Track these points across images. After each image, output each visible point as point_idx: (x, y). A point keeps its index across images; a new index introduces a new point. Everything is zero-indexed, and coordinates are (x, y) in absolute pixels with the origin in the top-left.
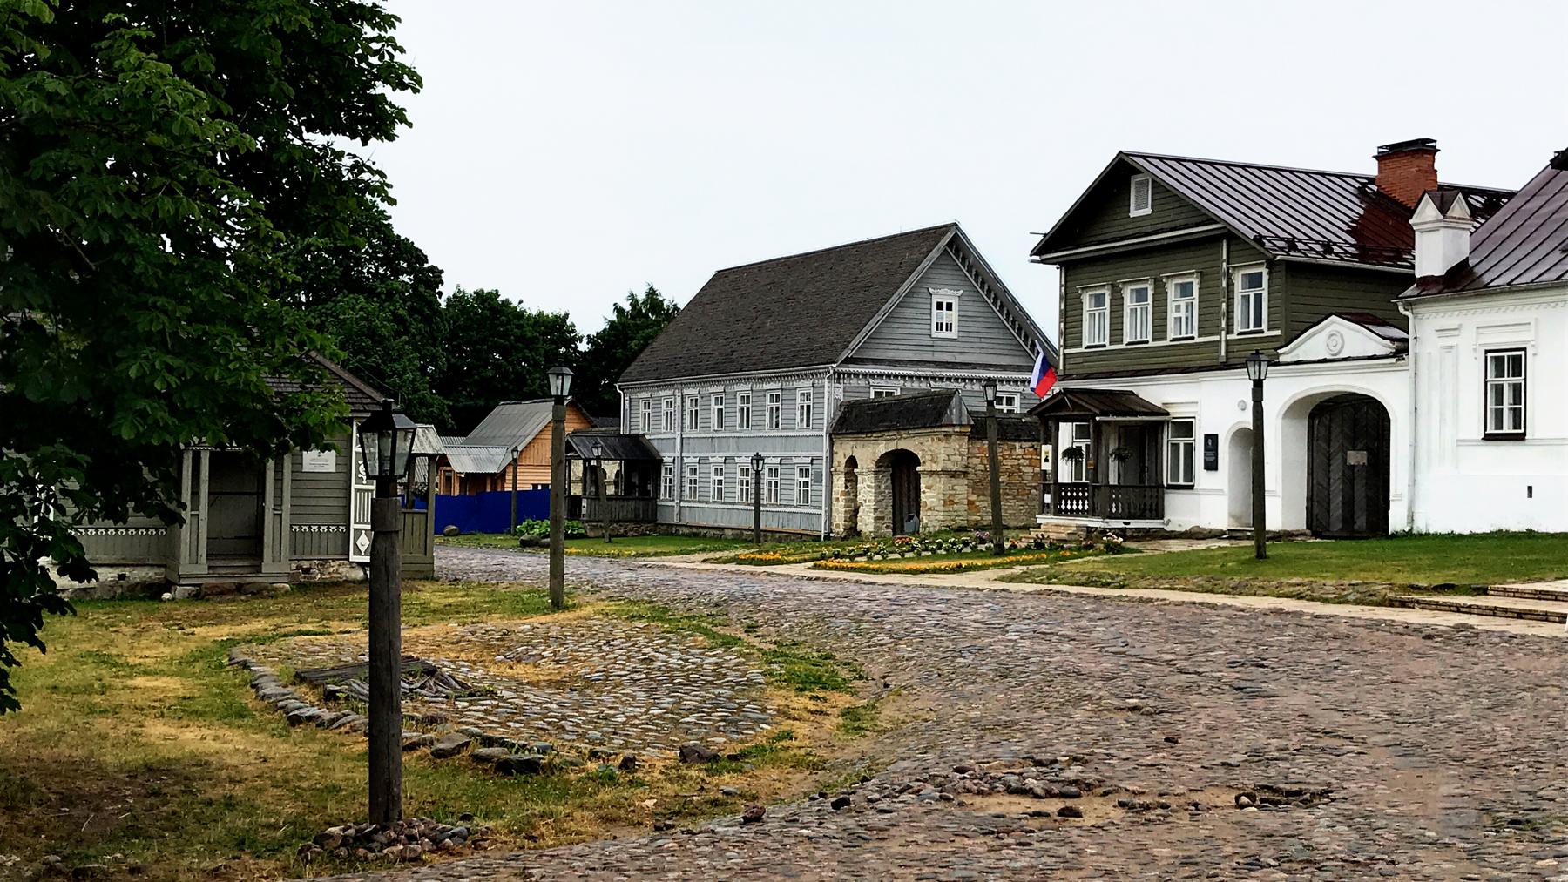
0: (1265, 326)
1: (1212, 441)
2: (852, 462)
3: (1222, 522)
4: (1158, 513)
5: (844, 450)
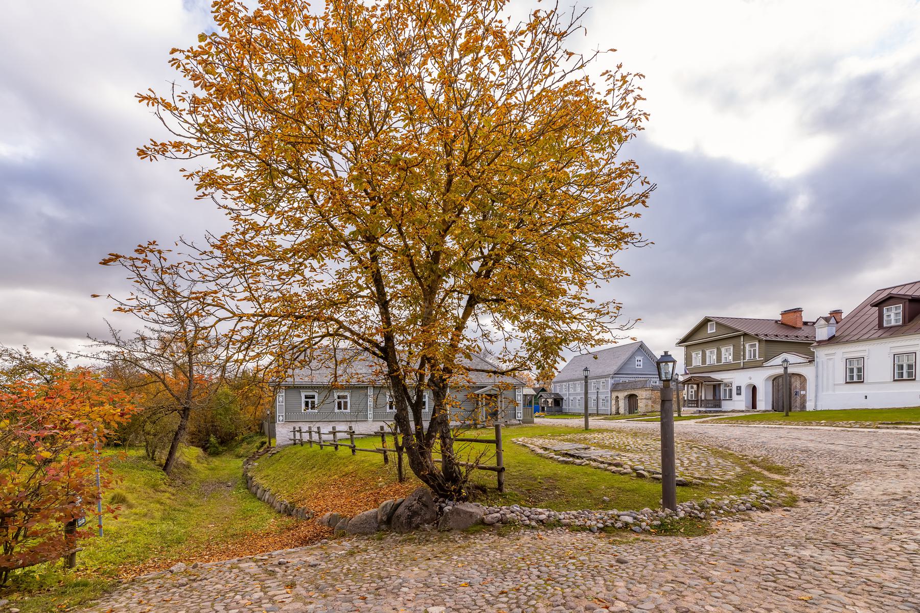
0: (757, 357)
1: (739, 389)
2: (617, 397)
3: (744, 408)
4: (720, 407)
5: (614, 395)
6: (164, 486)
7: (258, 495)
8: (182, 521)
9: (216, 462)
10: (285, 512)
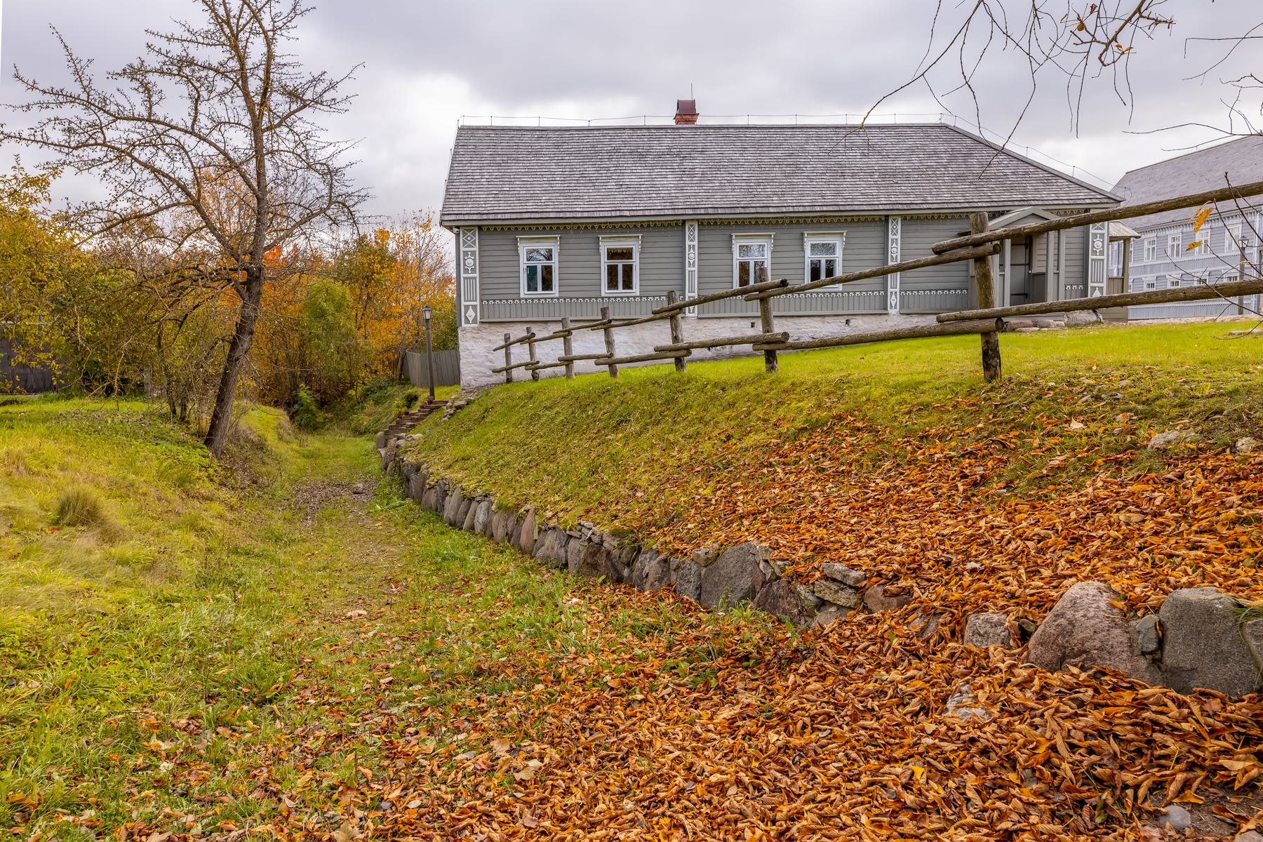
6: (208, 484)
7: (449, 512)
8: (262, 592)
9: (314, 443)
10: (594, 567)
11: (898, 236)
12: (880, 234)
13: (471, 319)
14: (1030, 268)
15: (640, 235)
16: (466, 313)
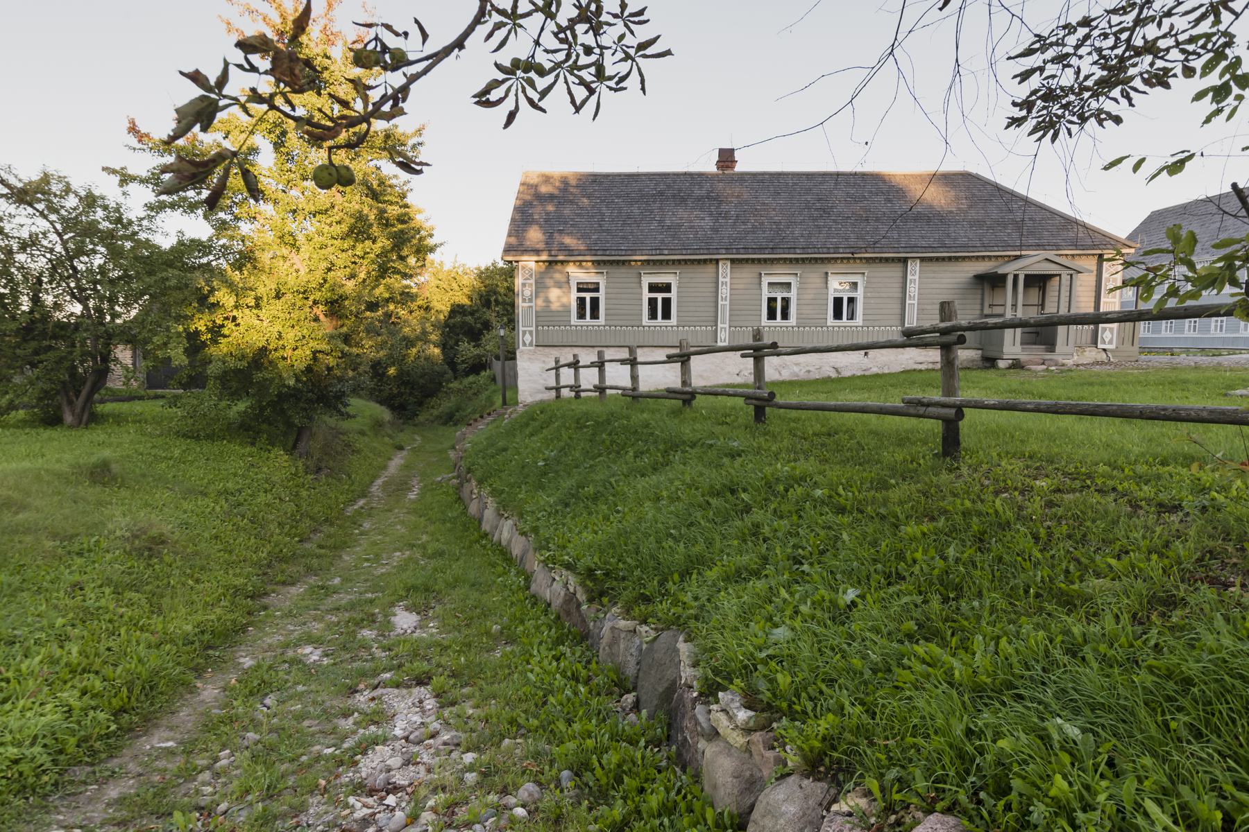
11: (917, 277)
12: (901, 269)
13: (527, 343)
14: (1043, 309)
15: (799, 272)
16: (1102, 334)
